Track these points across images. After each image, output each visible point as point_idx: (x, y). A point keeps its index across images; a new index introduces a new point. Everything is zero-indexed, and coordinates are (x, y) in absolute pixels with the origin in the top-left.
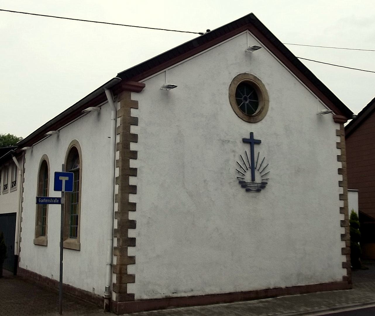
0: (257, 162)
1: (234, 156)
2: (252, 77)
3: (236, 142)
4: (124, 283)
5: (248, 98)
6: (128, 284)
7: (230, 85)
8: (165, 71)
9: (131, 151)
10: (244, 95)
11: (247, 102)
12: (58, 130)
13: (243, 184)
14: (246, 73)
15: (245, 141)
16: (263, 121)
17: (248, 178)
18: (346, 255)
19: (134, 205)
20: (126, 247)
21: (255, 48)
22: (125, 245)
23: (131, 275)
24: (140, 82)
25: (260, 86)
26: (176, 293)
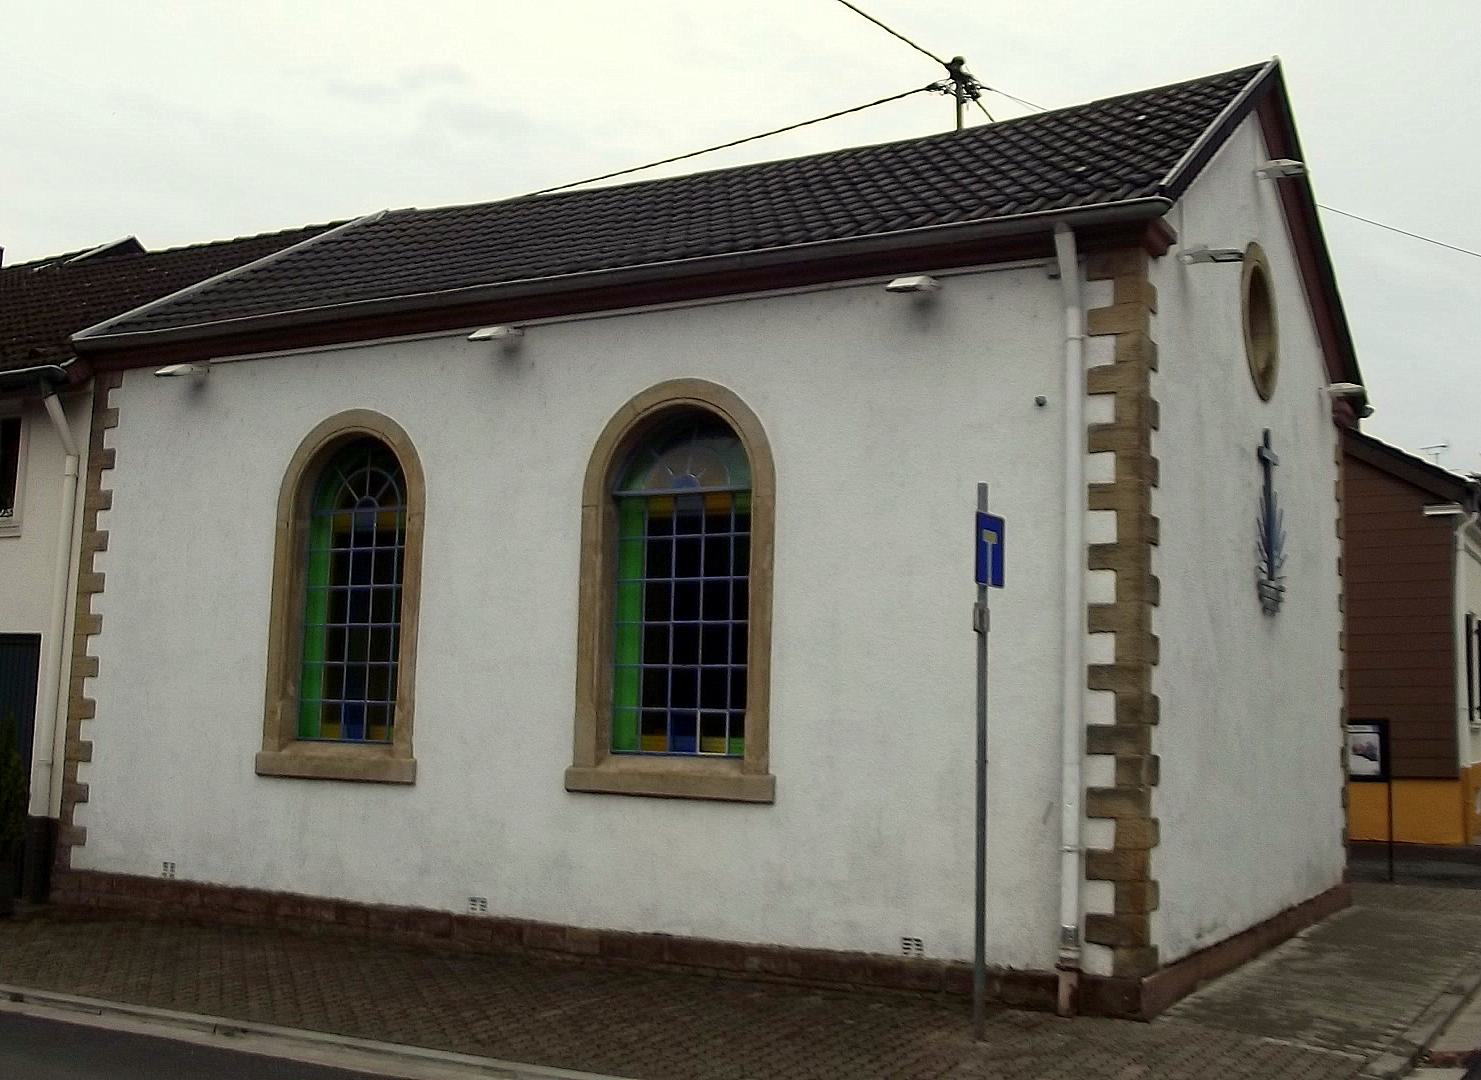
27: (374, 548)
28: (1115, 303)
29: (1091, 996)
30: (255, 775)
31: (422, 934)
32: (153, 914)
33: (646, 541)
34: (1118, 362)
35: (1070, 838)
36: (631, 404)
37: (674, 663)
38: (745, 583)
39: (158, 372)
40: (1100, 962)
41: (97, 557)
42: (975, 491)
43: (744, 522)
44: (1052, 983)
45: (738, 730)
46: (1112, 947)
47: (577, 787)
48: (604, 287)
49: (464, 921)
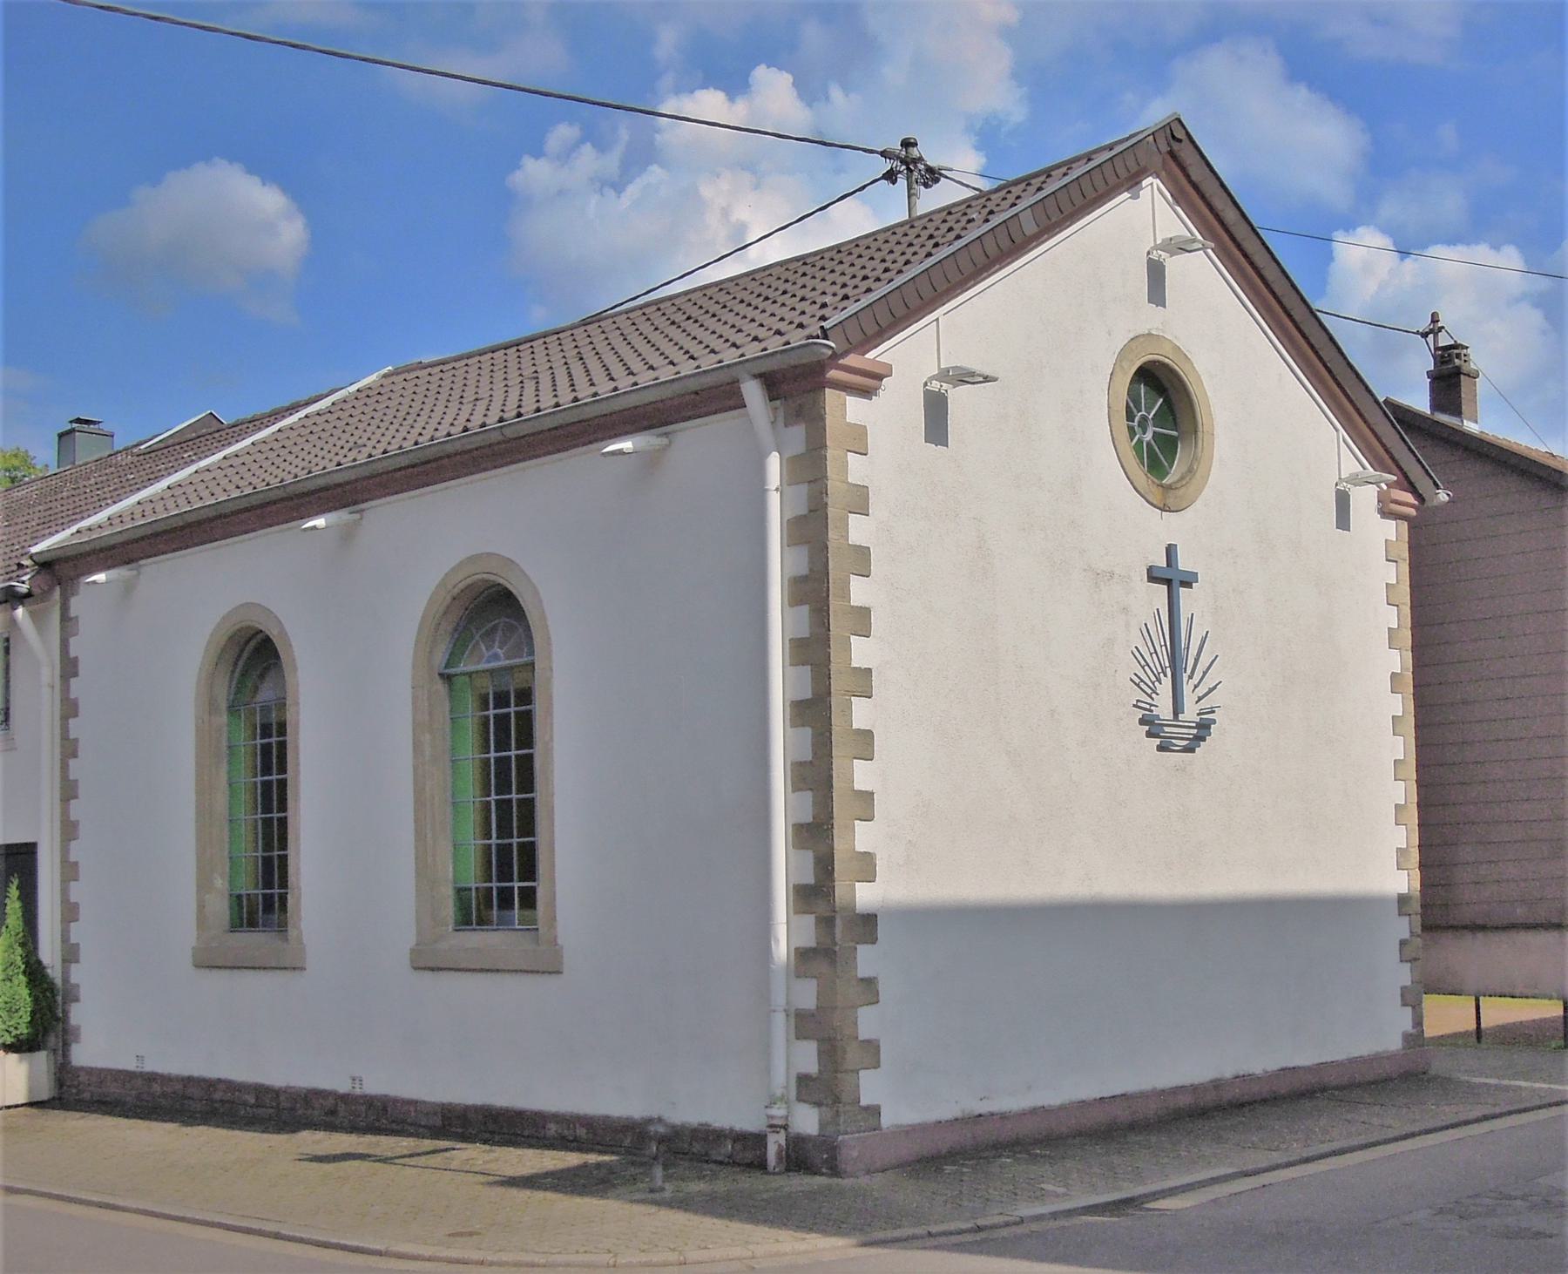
0: (1197, 660)
1: (1127, 625)
2: (1167, 350)
3: (1129, 577)
4: (852, 1071)
5: (1150, 423)
6: (862, 1073)
7: (1112, 374)
8: (937, 320)
9: (853, 607)
10: (1138, 412)
11: (1148, 436)
12: (744, 358)
13: (1151, 725)
14: (1150, 334)
15: (1153, 576)
16: (1198, 504)
17: (1164, 709)
18: (1410, 961)
19: (867, 736)
20: (847, 635)
21: (1179, 247)
22: (852, 941)
23: (868, 1042)
24: (871, 355)
25: (1193, 388)
26: (988, 1099)
27: (512, 709)
28: (807, 450)
29: (799, 1157)
30: (194, 968)
31: (316, 1113)
32: (362, 1123)
33: (259, 747)
34: (811, 511)
35: (779, 999)
36: (443, 583)
37: (498, 838)
38: (530, 757)
39: (88, 580)
40: (807, 1121)
41: (72, 762)
42: (1188, 580)
43: (525, 696)
44: (759, 1140)
45: (529, 899)
46: (818, 1104)
47: (426, 963)
48: (711, 388)
49: (345, 1098)
